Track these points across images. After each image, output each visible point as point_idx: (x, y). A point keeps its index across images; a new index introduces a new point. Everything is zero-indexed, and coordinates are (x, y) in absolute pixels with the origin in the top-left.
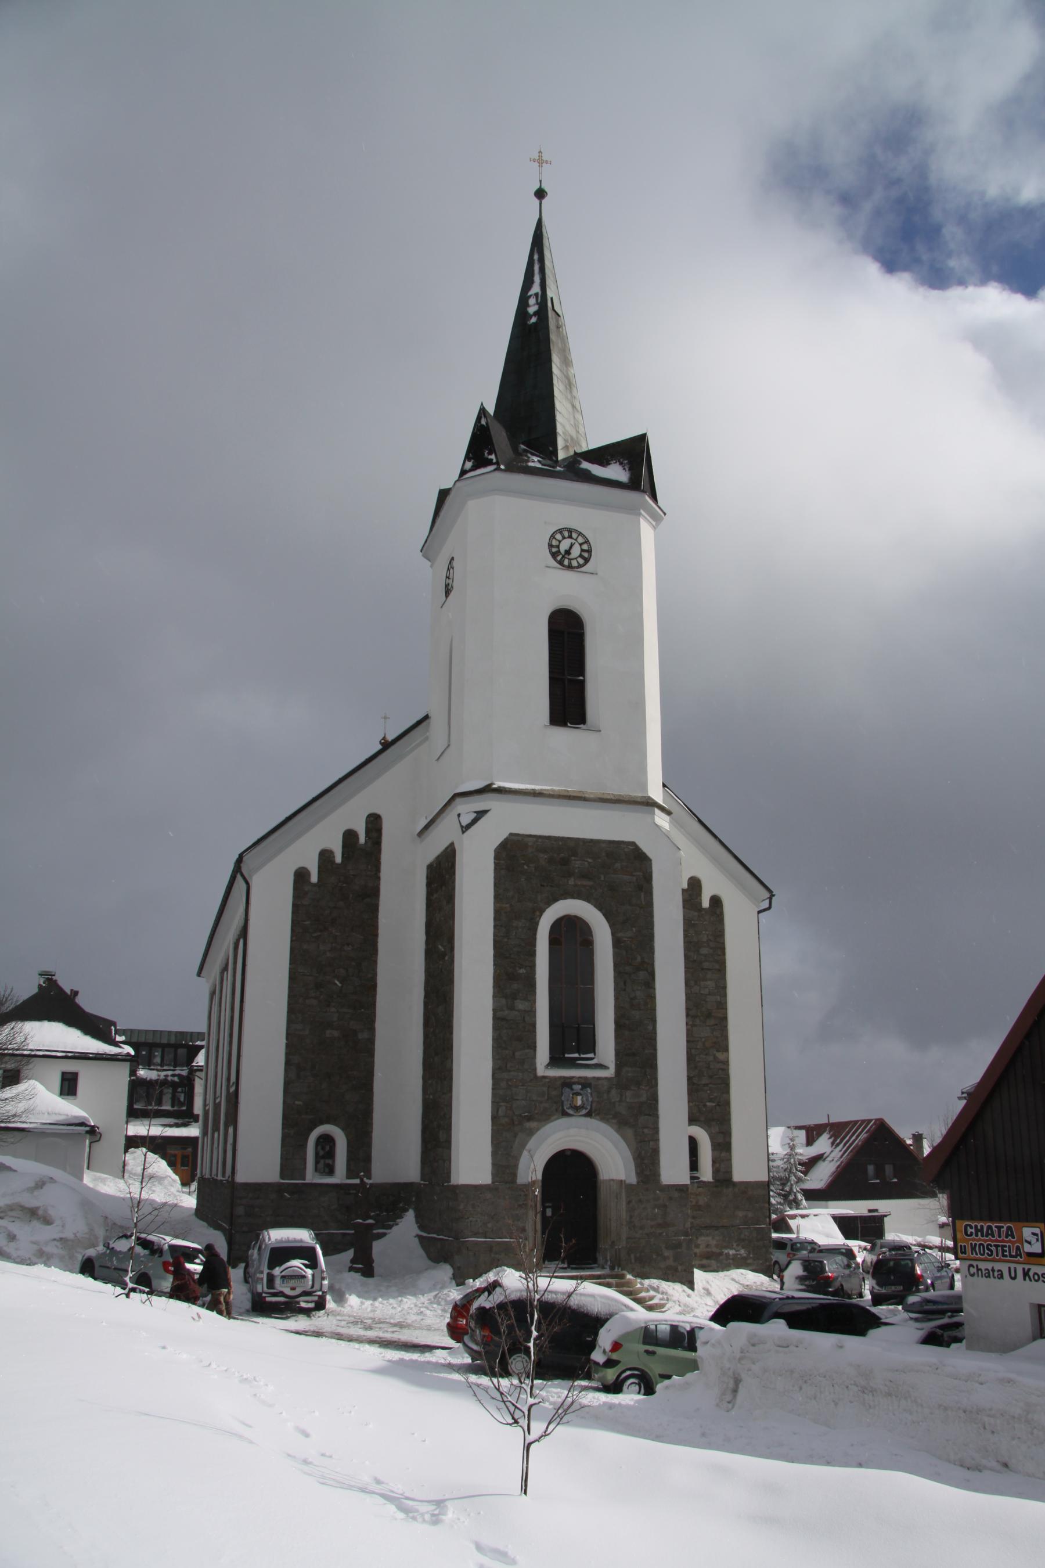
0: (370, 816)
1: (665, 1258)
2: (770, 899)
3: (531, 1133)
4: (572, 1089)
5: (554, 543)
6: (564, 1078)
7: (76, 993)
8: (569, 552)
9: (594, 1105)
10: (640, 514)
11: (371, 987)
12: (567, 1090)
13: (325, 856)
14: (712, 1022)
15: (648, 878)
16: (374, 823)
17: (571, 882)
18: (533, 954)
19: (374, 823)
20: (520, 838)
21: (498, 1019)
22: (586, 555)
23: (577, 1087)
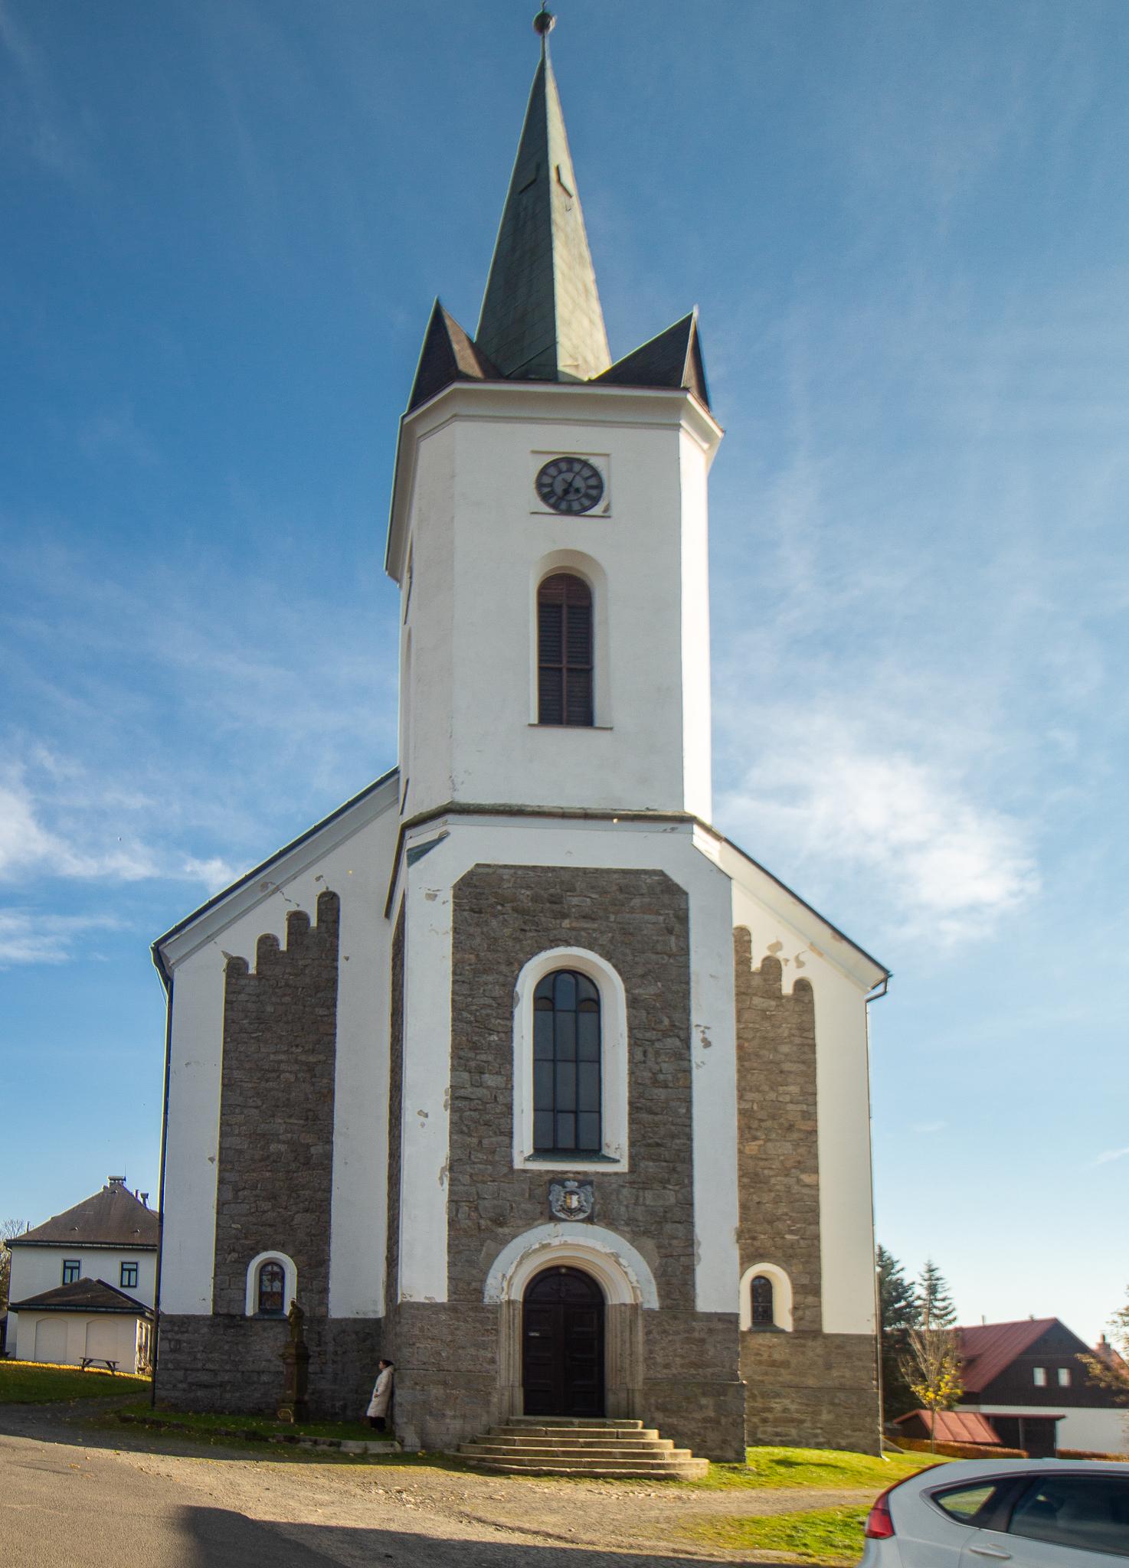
1: (701, 1407)
2: (885, 981)
6: (553, 1172)
8: (570, 487)
9: (597, 1207)
10: (679, 426)
12: (557, 1188)
13: (267, 943)
14: (795, 1136)
15: (683, 919)
16: (329, 902)
17: (566, 923)
19: (329, 902)
20: (490, 871)
23: (572, 1185)
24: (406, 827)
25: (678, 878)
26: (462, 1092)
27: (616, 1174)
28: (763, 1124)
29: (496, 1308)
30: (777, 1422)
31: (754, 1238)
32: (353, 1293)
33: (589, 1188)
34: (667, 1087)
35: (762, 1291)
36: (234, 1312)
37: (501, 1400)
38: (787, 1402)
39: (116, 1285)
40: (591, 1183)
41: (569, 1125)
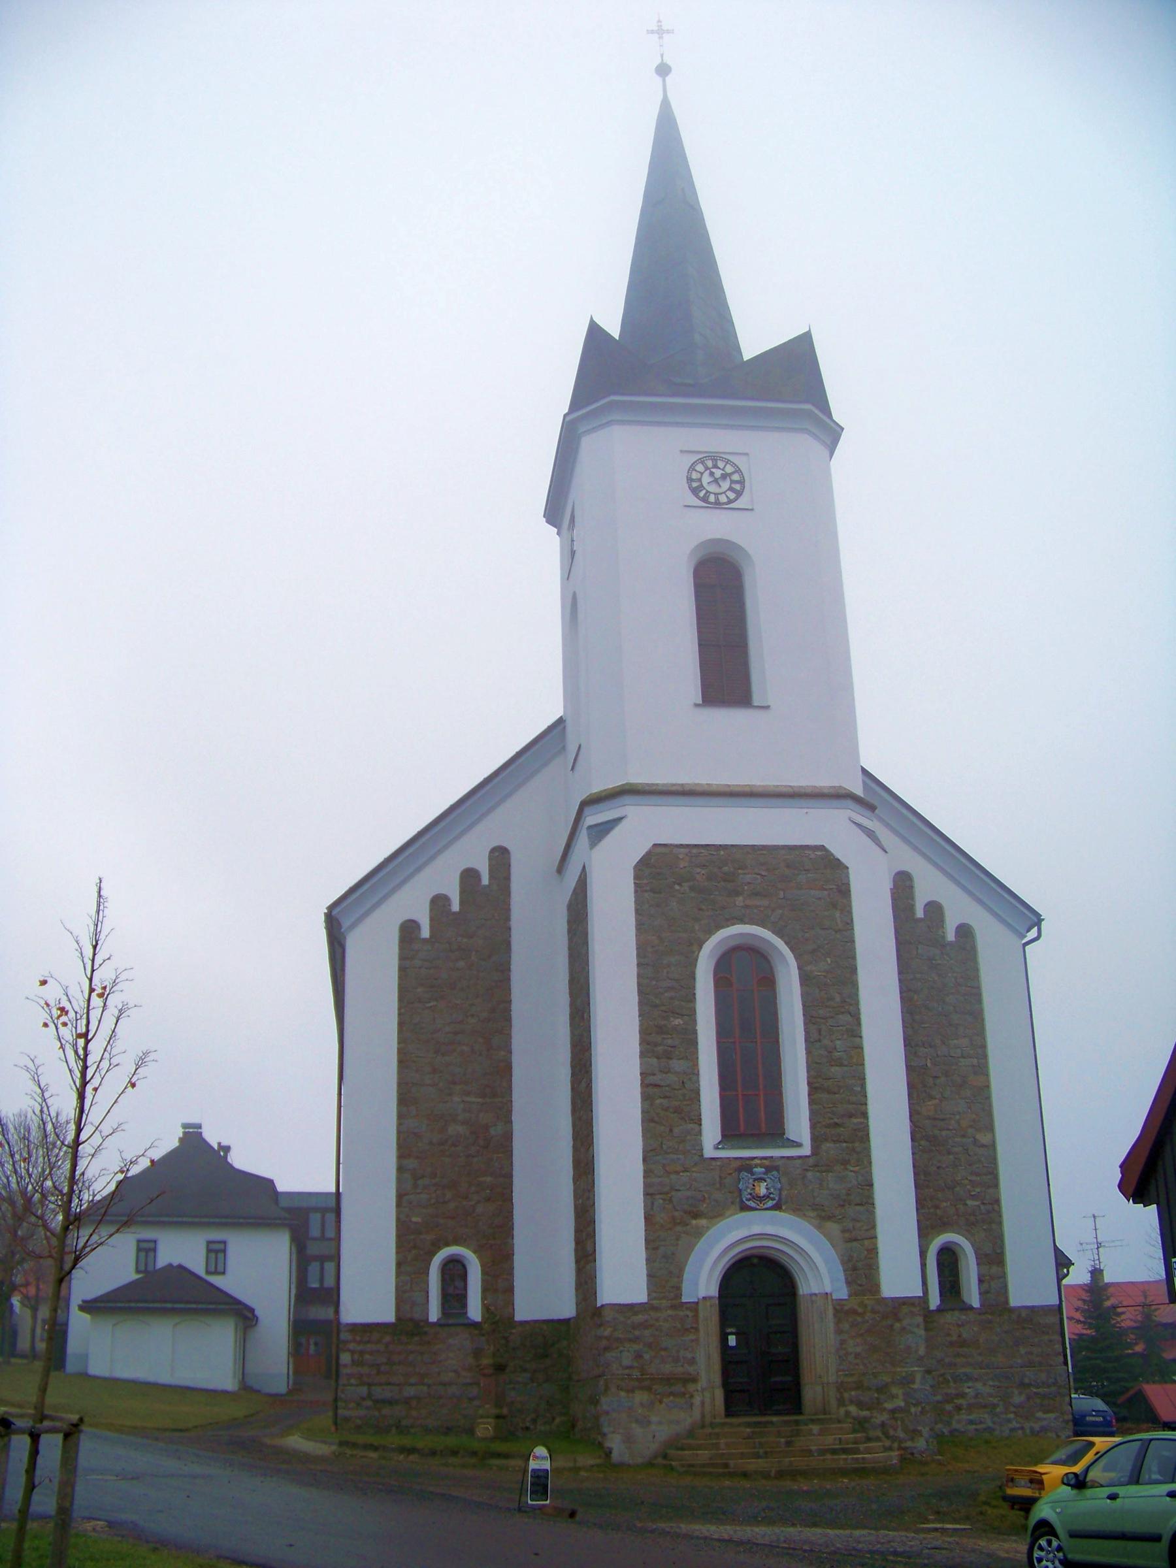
0: (493, 850)
3: (699, 1233)
4: (752, 1174)
5: (695, 476)
7: (227, 1149)
9: (784, 1193)
11: (505, 1070)
12: (744, 1174)
13: (439, 903)
15: (844, 891)
16: (500, 857)
17: (739, 901)
18: (691, 998)
19: (500, 857)
21: (648, 1086)
22: (738, 487)
24: (584, 804)
25: (838, 853)
26: (651, 1079)
27: (800, 1157)
28: (938, 1081)
29: (694, 1306)
30: (970, 1407)
31: (937, 1207)
32: (542, 1292)
33: (775, 1173)
34: (842, 1065)
35: (948, 1260)
36: (417, 1316)
37: (703, 1403)
38: (979, 1385)
39: (200, 1270)
40: (776, 1168)
41: (752, 1107)
